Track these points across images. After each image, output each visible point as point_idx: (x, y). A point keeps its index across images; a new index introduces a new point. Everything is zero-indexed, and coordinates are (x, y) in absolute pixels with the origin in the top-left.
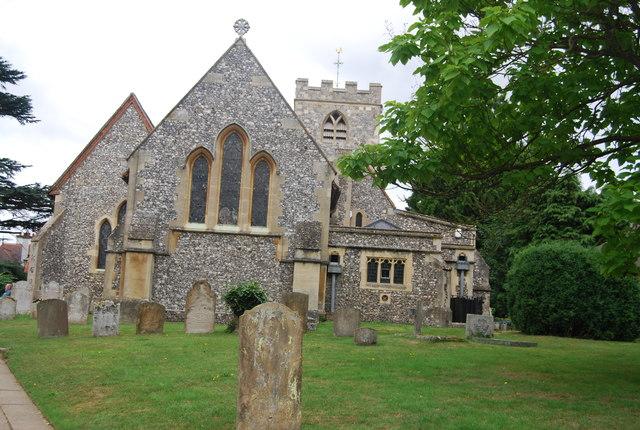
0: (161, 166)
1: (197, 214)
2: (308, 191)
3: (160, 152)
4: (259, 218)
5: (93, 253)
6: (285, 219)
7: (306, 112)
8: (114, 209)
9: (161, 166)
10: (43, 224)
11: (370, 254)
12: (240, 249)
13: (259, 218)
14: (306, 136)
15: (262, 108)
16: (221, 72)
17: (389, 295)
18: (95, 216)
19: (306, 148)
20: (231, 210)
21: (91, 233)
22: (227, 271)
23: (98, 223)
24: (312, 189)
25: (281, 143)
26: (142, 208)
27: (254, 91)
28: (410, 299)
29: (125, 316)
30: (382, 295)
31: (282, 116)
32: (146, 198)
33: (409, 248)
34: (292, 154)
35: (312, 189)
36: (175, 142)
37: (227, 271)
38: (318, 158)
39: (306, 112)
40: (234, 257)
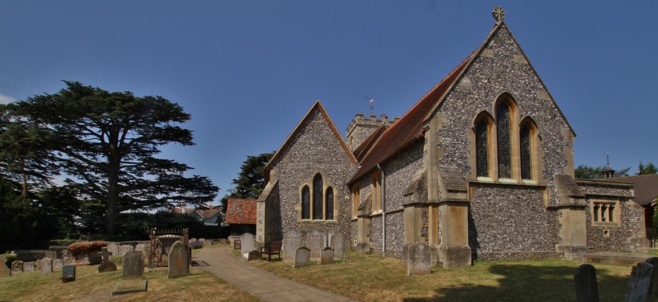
0: (455, 126)
1: (482, 169)
2: (559, 151)
3: (453, 115)
4: (526, 174)
5: (299, 208)
6: (546, 172)
7: (363, 131)
8: (311, 179)
9: (455, 126)
10: (424, 177)
11: (595, 200)
12: (518, 198)
13: (526, 174)
14: (553, 106)
15: (523, 82)
16: (491, 48)
17: (608, 230)
18: (298, 183)
19: (555, 116)
20: (506, 166)
21: (297, 195)
22: (511, 216)
23: (301, 188)
24: (562, 149)
25: (538, 111)
26: (443, 164)
27: (516, 67)
28: (620, 232)
29: (453, 261)
30: (604, 230)
31: (537, 89)
32: (446, 154)
33: (616, 195)
34: (546, 120)
35: (562, 149)
36: (463, 106)
37: (511, 216)
38: (563, 124)
39: (363, 131)
40: (516, 205)
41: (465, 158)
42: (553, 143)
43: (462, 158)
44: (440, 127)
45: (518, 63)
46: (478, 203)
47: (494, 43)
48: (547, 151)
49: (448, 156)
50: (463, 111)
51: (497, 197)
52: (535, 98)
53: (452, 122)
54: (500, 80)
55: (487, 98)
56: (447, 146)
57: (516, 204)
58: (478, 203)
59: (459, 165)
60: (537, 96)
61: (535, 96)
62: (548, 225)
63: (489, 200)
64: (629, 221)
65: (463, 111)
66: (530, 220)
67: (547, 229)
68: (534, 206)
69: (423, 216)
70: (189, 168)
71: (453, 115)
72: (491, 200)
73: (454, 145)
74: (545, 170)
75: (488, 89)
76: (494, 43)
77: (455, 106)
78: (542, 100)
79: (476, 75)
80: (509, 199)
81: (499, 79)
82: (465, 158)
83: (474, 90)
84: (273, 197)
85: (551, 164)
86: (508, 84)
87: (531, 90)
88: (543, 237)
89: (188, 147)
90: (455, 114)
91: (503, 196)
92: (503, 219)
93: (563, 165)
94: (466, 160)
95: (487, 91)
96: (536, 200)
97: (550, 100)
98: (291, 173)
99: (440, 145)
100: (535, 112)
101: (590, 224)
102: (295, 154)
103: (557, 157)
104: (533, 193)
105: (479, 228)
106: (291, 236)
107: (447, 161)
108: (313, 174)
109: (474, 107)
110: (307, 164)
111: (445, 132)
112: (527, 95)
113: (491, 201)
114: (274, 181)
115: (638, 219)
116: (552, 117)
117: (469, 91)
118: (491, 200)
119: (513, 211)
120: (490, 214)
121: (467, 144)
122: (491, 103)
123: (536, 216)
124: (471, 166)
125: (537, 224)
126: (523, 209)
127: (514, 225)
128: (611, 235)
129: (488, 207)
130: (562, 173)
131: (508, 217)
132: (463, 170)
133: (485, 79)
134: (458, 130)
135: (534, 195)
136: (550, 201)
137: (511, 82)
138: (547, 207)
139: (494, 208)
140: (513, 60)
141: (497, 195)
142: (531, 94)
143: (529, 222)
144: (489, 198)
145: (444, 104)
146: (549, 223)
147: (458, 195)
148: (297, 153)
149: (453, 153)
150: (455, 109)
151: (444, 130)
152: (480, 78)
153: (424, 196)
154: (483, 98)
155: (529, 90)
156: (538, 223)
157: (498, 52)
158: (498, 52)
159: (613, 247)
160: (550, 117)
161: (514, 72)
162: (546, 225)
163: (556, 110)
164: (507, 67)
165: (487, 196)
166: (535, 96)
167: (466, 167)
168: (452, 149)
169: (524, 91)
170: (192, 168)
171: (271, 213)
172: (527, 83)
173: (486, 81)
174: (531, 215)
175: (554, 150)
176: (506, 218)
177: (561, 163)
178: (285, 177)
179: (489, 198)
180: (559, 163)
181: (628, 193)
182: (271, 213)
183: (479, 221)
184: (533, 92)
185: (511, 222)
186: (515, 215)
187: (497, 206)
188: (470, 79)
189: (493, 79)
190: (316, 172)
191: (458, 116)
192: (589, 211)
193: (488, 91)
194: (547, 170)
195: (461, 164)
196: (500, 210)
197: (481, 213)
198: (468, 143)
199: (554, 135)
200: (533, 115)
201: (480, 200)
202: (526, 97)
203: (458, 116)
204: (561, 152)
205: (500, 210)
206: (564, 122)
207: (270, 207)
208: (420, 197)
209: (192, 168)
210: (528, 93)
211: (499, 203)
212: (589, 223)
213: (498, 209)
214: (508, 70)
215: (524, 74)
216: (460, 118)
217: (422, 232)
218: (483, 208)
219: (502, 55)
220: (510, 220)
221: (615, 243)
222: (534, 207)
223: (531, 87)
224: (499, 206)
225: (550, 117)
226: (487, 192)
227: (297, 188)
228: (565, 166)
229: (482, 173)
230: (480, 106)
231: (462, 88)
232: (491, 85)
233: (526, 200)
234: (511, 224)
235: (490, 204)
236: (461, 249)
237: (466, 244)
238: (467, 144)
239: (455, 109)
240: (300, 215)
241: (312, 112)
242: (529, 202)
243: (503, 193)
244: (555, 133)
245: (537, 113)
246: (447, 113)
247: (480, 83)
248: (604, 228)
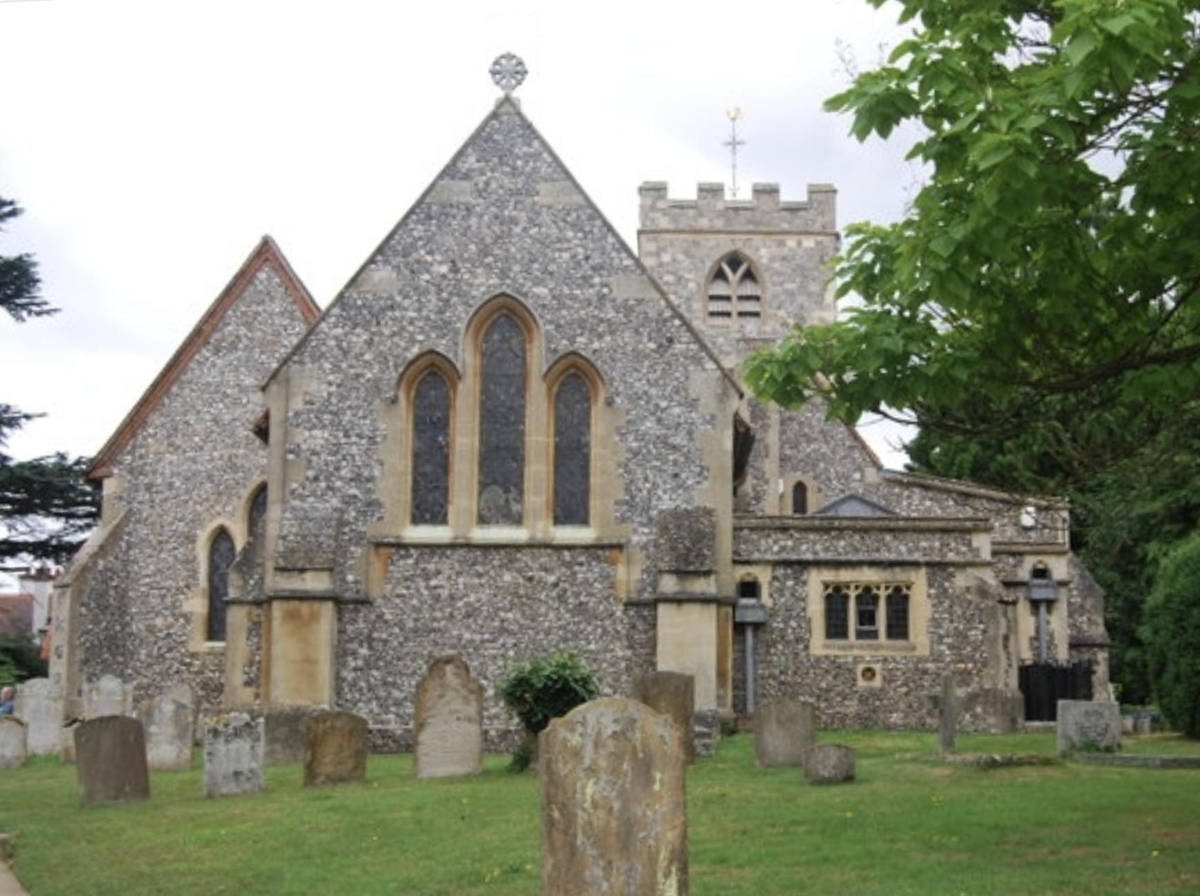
2: (679, 439)
3: (336, 368)
5: (197, 605)
7: (666, 258)
9: (342, 398)
11: (829, 575)
12: (530, 579)
14: (668, 314)
16: (466, 176)
17: (877, 667)
18: (197, 521)
19: (670, 341)
20: (507, 491)
25: (612, 333)
26: (302, 498)
27: (545, 217)
28: (925, 672)
31: (613, 270)
32: (311, 474)
33: (917, 556)
34: (639, 356)
36: (370, 343)
37: (503, 630)
38: (698, 361)
39: (666, 258)
41: (370, 480)
42: (659, 421)
43: (357, 479)
44: (297, 404)
45: (550, 207)
46: (398, 596)
47: (478, 161)
48: (635, 445)
49: (316, 479)
50: (368, 357)
51: (461, 580)
52: (602, 298)
53: (333, 389)
54: (489, 259)
55: (443, 313)
56: (314, 453)
57: (521, 597)
58: (398, 596)
59: (349, 500)
60: (611, 291)
61: (605, 290)
62: (629, 653)
63: (435, 587)
64: (966, 637)
65: (368, 357)
66: (565, 640)
67: (623, 665)
68: (583, 599)
69: (250, 632)
70: (27, 417)
71: (336, 368)
72: (442, 587)
73: (336, 449)
74: (627, 498)
75: (450, 289)
76: (478, 161)
77: (344, 344)
78: (627, 300)
79: (415, 255)
80: (500, 584)
81: (486, 256)
82: (370, 480)
83: (406, 297)
84: (107, 569)
85: (646, 479)
86: (517, 268)
87: (591, 277)
88: (610, 686)
89: (33, 322)
90: (344, 365)
91: (480, 575)
92: (477, 637)
93: (690, 482)
94: (370, 485)
95: (445, 295)
96: (591, 585)
97: (656, 295)
98: (171, 486)
99: (296, 451)
100: (600, 336)
101: (807, 647)
102: (187, 423)
103: (671, 457)
104: (581, 564)
105: (401, 663)
106: (35, 690)
107: (315, 491)
108: (244, 486)
109: (403, 344)
110: (226, 453)
111: (312, 416)
112: (577, 292)
113: (440, 591)
114: (113, 519)
115: (984, 632)
116: (660, 346)
117: (389, 302)
118: (442, 587)
119: (510, 615)
120: (435, 625)
121: (376, 443)
122: (459, 325)
123: (590, 629)
124: (382, 499)
125: (591, 652)
126: (543, 610)
127: (511, 653)
128: (888, 680)
129: (432, 608)
130: (687, 502)
131: (492, 633)
132: (358, 512)
133: (441, 263)
134: (350, 407)
135: (584, 569)
136: (639, 586)
137: (526, 260)
138: (625, 600)
139: (448, 610)
140: (536, 198)
141: (459, 574)
142: (592, 286)
143: (562, 646)
144: (433, 583)
145: (314, 344)
146: (631, 647)
147: (303, 580)
148: (191, 418)
149: (331, 469)
150: (345, 353)
151: (309, 411)
152: (426, 262)
153: (256, 583)
154: (433, 316)
155: (584, 278)
156: (592, 647)
157: (487, 184)
158: (487, 184)
159: (895, 718)
160: (652, 346)
161: (539, 233)
162: (620, 654)
163: (677, 322)
164: (514, 221)
165: (427, 578)
166: (605, 290)
167: (369, 504)
168: (330, 458)
169: (568, 280)
170: (42, 415)
171: (96, 622)
172: (580, 257)
173: (444, 269)
174: (571, 627)
175: (664, 441)
176: (487, 636)
177: (683, 476)
178: (153, 501)
179: (433, 583)
180: (676, 476)
181: (964, 549)
182: (96, 622)
183: (401, 644)
184: (597, 280)
185: (503, 645)
186: (514, 627)
187: (460, 604)
188: (397, 268)
189: (468, 260)
190: (256, 480)
191: (352, 371)
192: (804, 609)
193: (451, 294)
194: (633, 498)
195: (355, 497)
196: (468, 615)
197: (410, 624)
198: (378, 439)
199: (664, 397)
200: (596, 345)
201: (408, 588)
202: (574, 298)
203: (352, 371)
204: (685, 442)
205: (468, 615)
206: (703, 354)
207: (93, 605)
208: (246, 582)
209: (42, 415)
210: (579, 286)
211: (466, 595)
212: (801, 646)
213: (463, 611)
214: (517, 230)
215: (570, 234)
216: (358, 376)
217: (245, 673)
218: (417, 610)
219: (501, 192)
220: (501, 641)
221: (902, 706)
222: (581, 604)
223: (593, 268)
224: (467, 605)
225: (652, 346)
226: (431, 567)
227: (191, 539)
228: (698, 483)
229: (428, 516)
230: (420, 338)
231: (369, 296)
232: (459, 276)
233: (556, 585)
234: (502, 651)
235: (437, 598)
236: (304, 714)
237: (323, 703)
238: (376, 443)
239: (345, 353)
240: (198, 628)
241: (244, 277)
242: (565, 591)
243: (479, 568)
244: (669, 389)
245: (608, 338)
246: (321, 368)
247: (426, 277)
248: (857, 660)
